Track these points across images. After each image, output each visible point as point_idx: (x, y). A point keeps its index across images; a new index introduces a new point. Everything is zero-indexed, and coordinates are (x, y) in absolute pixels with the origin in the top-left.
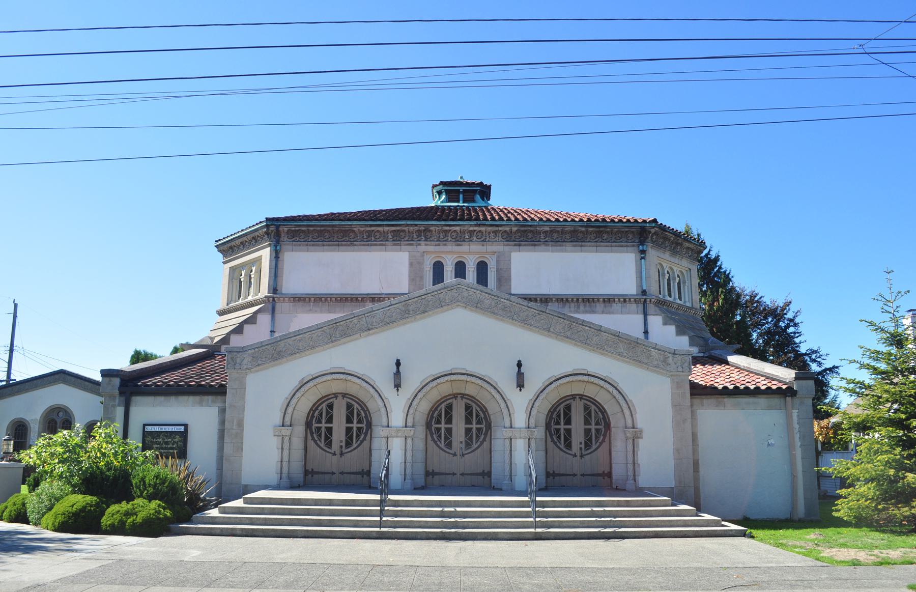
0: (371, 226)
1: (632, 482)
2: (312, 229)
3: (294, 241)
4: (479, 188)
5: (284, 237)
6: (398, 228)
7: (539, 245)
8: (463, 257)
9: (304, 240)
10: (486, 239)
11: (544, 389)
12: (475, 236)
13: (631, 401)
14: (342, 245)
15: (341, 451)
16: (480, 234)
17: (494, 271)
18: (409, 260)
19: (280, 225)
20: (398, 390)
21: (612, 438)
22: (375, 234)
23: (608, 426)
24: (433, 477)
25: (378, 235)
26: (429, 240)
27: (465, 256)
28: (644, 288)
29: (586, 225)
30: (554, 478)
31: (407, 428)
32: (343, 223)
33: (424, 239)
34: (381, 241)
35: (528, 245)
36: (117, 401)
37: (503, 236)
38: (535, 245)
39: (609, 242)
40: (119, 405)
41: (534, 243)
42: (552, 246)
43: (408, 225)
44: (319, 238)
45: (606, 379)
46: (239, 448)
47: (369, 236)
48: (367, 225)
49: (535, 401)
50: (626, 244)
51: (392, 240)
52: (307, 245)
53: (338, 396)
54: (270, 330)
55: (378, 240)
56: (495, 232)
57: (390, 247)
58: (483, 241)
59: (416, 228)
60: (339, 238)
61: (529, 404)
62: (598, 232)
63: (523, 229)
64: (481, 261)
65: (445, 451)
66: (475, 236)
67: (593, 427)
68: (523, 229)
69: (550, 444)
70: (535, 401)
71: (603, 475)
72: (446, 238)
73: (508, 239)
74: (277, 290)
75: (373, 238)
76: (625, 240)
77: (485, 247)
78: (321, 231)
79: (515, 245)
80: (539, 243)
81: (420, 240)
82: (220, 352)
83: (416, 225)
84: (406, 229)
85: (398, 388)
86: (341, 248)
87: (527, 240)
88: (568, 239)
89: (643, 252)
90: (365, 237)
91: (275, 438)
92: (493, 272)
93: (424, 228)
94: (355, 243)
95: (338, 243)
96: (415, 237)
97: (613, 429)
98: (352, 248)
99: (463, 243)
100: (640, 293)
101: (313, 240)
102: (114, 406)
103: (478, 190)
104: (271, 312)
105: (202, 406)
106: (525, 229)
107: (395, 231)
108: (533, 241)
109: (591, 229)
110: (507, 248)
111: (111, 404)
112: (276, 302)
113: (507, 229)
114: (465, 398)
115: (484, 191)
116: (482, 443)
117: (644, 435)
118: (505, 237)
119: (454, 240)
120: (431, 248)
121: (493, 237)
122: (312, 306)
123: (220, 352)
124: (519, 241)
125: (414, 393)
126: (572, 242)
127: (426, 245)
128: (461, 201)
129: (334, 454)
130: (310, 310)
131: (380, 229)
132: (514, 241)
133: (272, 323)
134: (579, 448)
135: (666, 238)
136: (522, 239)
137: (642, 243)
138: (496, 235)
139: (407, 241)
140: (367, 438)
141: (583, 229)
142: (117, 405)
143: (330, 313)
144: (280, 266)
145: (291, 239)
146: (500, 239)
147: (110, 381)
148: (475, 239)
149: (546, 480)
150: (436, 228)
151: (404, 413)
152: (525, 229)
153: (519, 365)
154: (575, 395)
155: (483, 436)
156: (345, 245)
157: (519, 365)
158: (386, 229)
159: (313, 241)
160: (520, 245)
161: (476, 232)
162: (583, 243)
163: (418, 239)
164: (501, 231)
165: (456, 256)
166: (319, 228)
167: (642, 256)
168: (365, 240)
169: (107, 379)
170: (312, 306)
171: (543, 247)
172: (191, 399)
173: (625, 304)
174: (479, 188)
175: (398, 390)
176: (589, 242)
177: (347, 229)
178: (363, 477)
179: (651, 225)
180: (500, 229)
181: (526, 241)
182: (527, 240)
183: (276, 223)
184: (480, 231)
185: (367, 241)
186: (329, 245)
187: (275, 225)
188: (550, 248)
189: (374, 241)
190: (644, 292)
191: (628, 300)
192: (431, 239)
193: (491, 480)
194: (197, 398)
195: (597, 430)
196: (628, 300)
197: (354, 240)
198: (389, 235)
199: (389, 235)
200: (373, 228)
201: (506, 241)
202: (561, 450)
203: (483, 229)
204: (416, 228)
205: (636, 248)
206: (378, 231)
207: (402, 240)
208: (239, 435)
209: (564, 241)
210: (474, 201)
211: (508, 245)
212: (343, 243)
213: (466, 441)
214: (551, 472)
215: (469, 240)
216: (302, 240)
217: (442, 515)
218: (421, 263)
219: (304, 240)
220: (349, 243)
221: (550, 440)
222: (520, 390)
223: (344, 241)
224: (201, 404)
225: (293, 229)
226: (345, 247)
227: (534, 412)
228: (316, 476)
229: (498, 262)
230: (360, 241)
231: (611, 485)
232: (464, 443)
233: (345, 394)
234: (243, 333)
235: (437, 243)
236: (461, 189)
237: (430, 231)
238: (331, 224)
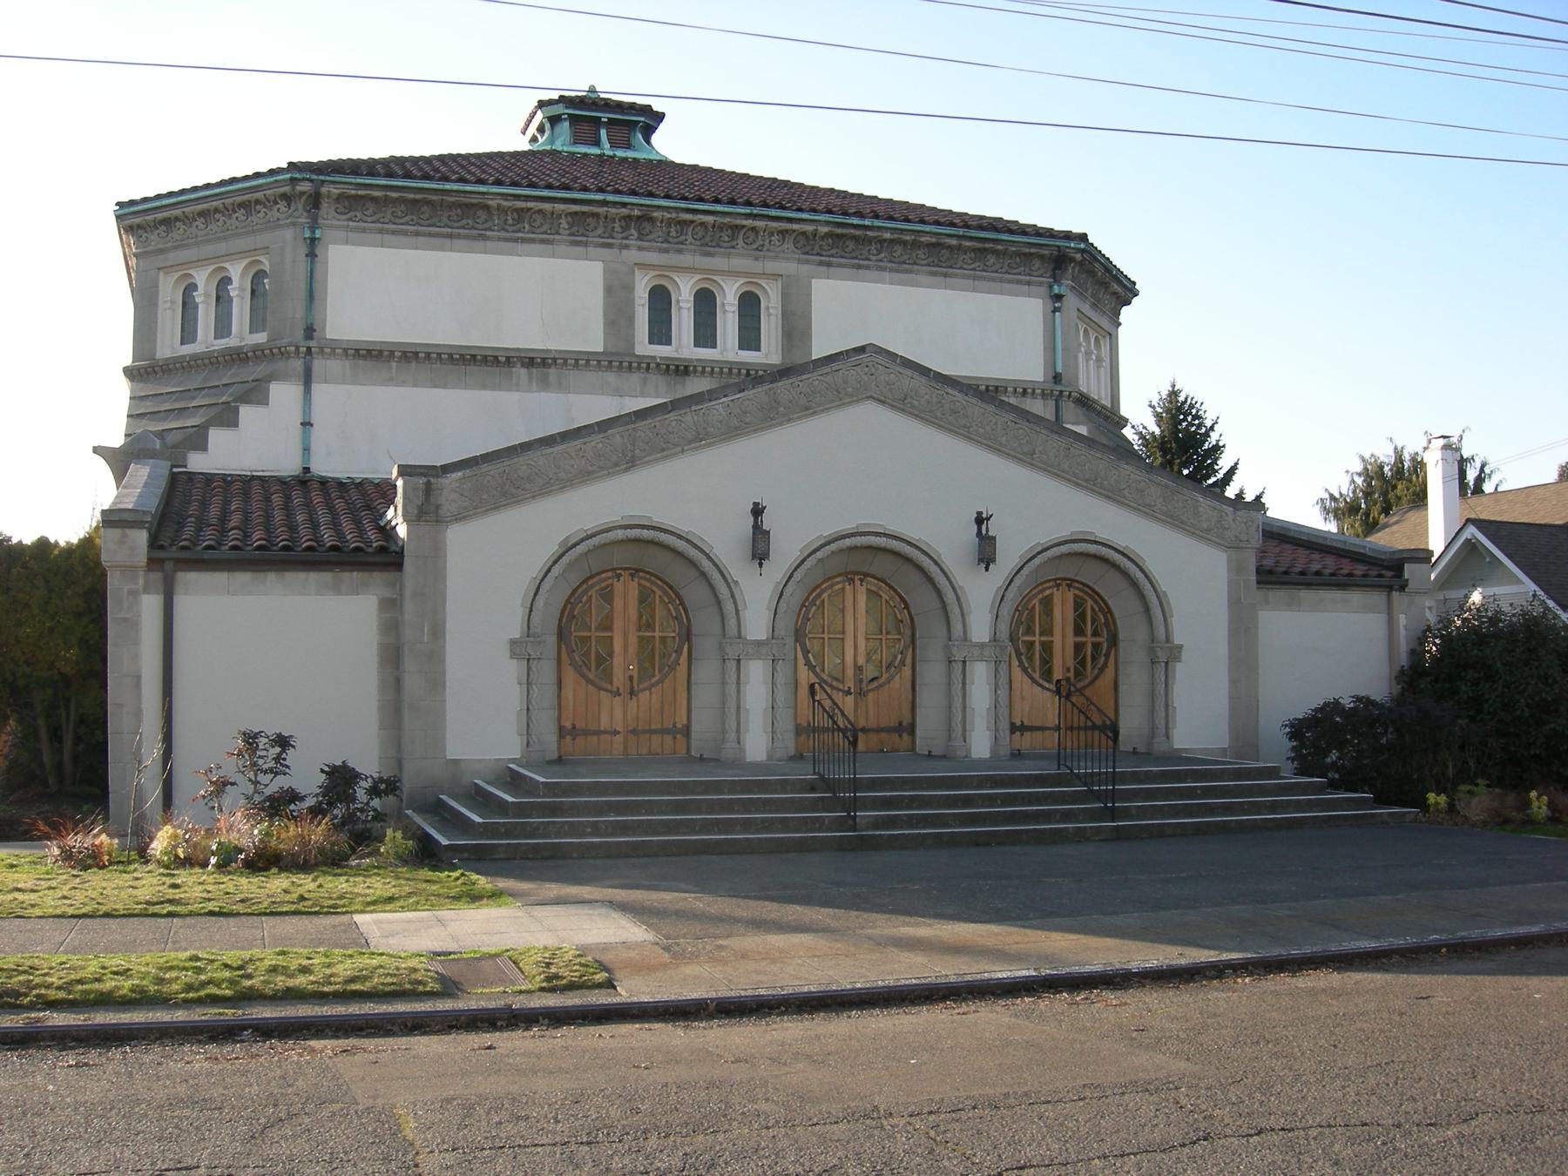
0: (527, 198)
1: (735, 745)
2: (394, 195)
3: (350, 219)
4: (642, 119)
5: (326, 208)
6: (585, 208)
7: (867, 267)
8: (760, 285)
9: (374, 218)
10: (763, 245)
11: (1021, 568)
12: (741, 236)
13: (962, 588)
14: (459, 236)
15: (861, 689)
16: (752, 235)
17: (777, 315)
18: (605, 279)
19: (323, 182)
20: (761, 565)
21: (1121, 660)
22: (531, 217)
23: (1114, 640)
24: (1022, 735)
25: (539, 219)
26: (646, 238)
27: (671, 274)
28: (1059, 369)
29: (961, 233)
30: (1022, 735)
31: (531, 639)
32: (468, 188)
33: (636, 235)
34: (545, 233)
35: (844, 266)
36: (141, 582)
37: (798, 242)
38: (859, 267)
39: (997, 272)
40: (146, 591)
41: (856, 261)
42: (891, 270)
43: (608, 202)
44: (464, 222)
45: (1126, 552)
46: (436, 683)
47: (519, 220)
48: (517, 197)
49: (542, 580)
50: (1028, 278)
51: (568, 232)
52: (381, 231)
53: (621, 575)
54: (300, 421)
55: (538, 231)
56: (783, 233)
57: (563, 248)
58: (757, 249)
59: (624, 211)
60: (397, 217)
61: (996, 595)
62: (979, 249)
63: (839, 231)
64: (702, 289)
65: (1041, 686)
66: (741, 236)
67: (1089, 639)
68: (839, 231)
69: (1017, 672)
70: (542, 580)
71: (672, 731)
72: (683, 238)
73: (808, 248)
74: (315, 331)
75: (527, 226)
76: (1027, 271)
77: (760, 264)
78: (415, 201)
79: (821, 263)
80: (866, 262)
81: (626, 238)
82: (185, 466)
83: (624, 205)
84: (602, 210)
85: (761, 559)
86: (457, 242)
87: (844, 254)
88: (724, 242)
89: (1059, 297)
90: (510, 222)
91: (514, 662)
92: (773, 318)
93: (639, 214)
94: (488, 233)
95: (449, 230)
96: (618, 229)
97: (1122, 645)
98: (481, 244)
99: (717, 250)
100: (1050, 378)
101: (393, 220)
102: (134, 593)
103: (640, 122)
104: (302, 379)
105: (339, 593)
106: (845, 231)
107: (576, 213)
108: (856, 258)
109: (968, 244)
110: (804, 268)
111: (126, 588)
112: (313, 358)
113: (809, 228)
114: (1075, 588)
115: (647, 119)
116: (1102, 670)
117: (1185, 655)
118: (700, 235)
119: (698, 243)
120: (652, 257)
121: (777, 243)
122: (394, 371)
123: (185, 466)
124: (829, 256)
125: (786, 573)
126: (929, 265)
127: (640, 249)
128: (606, 145)
129: (848, 693)
130: (391, 379)
131: (547, 206)
132: (818, 254)
133: (304, 404)
134: (627, 678)
135: (1092, 273)
136: (834, 251)
137: (1056, 280)
138: (784, 239)
139: (600, 236)
140: (1109, 664)
141: (954, 242)
142: (141, 589)
143: (436, 387)
144: (318, 275)
145: (346, 214)
146: (791, 246)
147: (124, 536)
148: (741, 242)
149: (559, 742)
150: (665, 214)
151: (770, 611)
152: (845, 231)
153: (757, 511)
154: (1059, 579)
155: (1103, 659)
156: (467, 237)
157: (757, 511)
158: (560, 207)
159: (395, 224)
160: (829, 265)
161: (744, 230)
162: (951, 271)
163: (624, 235)
164: (794, 231)
165: (699, 277)
166: (411, 196)
167: (1056, 305)
168: (510, 229)
169: (115, 533)
170: (394, 371)
171: (875, 274)
172: (314, 577)
173: (1023, 399)
174: (642, 119)
175: (761, 565)
176: (961, 268)
177: (473, 201)
178: (900, 736)
179: (1078, 246)
180: (795, 226)
181: (842, 257)
182: (844, 254)
183: (314, 177)
184: (753, 229)
185: (513, 232)
186: (430, 235)
187: (311, 181)
188: (887, 275)
189: (529, 232)
190: (1057, 378)
191: (1030, 391)
192: (651, 237)
193: (914, 741)
194: (327, 576)
195: (1096, 646)
196: (1030, 391)
197: (486, 226)
198: (563, 221)
199: (563, 221)
200: (530, 205)
201: (804, 254)
202: (589, 681)
203: (760, 224)
204: (624, 211)
205: (1044, 290)
206: (540, 211)
207: (591, 234)
208: (435, 657)
209: (915, 263)
210: (629, 146)
211: (807, 262)
212: (461, 231)
213: (1076, 668)
214: (1019, 723)
215: (729, 245)
216: (369, 219)
217: (678, 807)
218: (629, 289)
219: (374, 218)
220: (475, 232)
221: (804, 662)
222: (987, 569)
223: (463, 227)
224: (337, 590)
225: (353, 192)
226: (465, 242)
227: (540, 602)
228: (580, 740)
229: (785, 297)
230: (498, 231)
231: (913, 749)
232: (1072, 671)
233: (637, 570)
234: (236, 425)
235: (665, 245)
236: (605, 116)
237: (651, 220)
238: (441, 187)
